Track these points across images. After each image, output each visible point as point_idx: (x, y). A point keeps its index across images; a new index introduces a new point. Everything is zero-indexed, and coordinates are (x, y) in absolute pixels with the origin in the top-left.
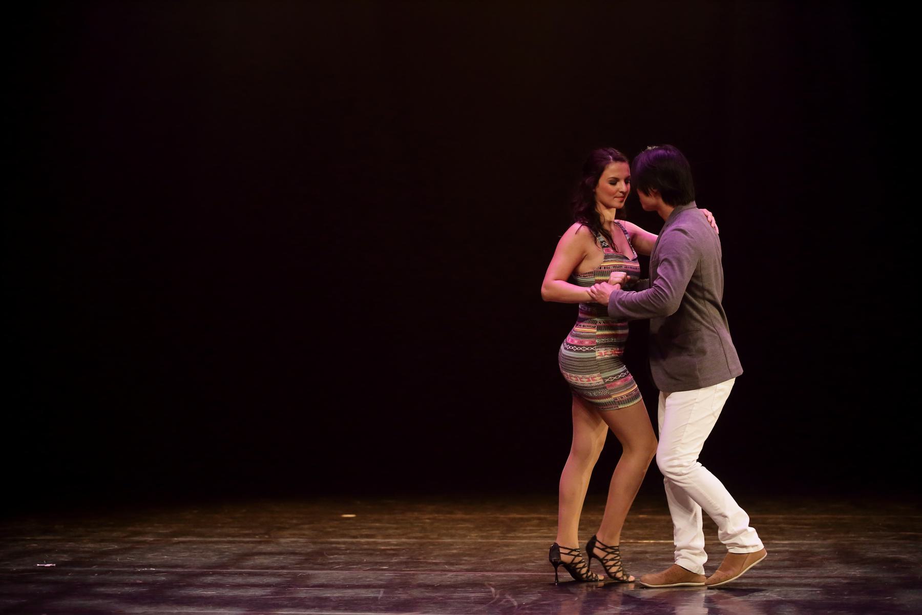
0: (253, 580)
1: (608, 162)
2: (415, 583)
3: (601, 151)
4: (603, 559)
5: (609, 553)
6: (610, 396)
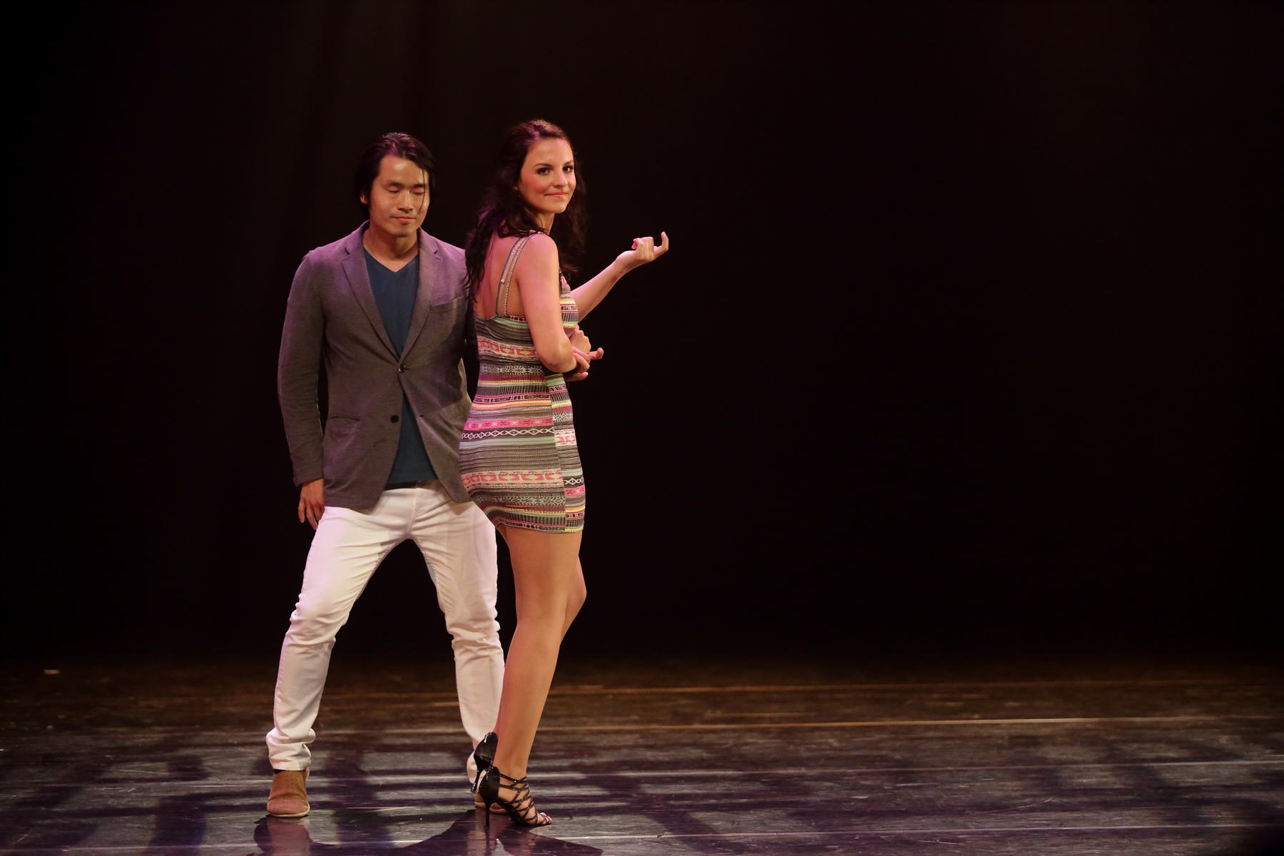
1: (386, 150)
2: (152, 817)
3: (524, 125)
4: (514, 801)
5: (519, 790)
6: (562, 508)
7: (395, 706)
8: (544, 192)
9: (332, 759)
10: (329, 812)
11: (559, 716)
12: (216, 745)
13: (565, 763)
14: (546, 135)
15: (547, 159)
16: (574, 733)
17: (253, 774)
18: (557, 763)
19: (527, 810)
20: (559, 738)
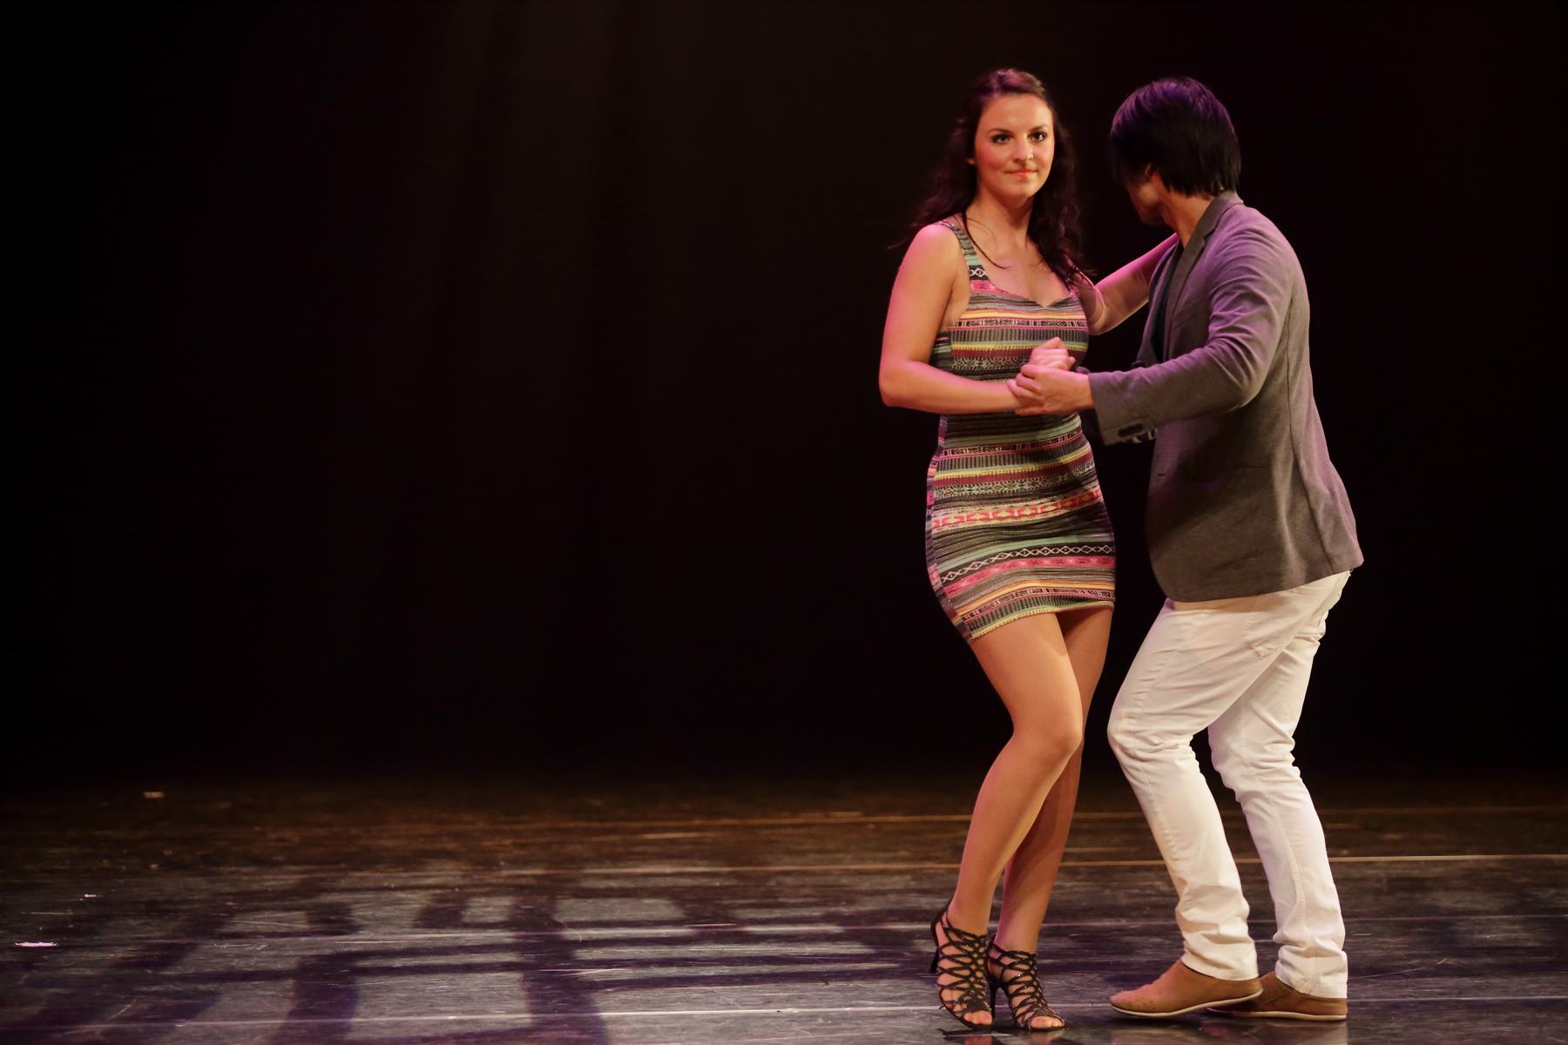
0: (790, 831)
7: (594, 839)
8: (996, 167)
9: (517, 907)
10: (516, 976)
11: (809, 851)
12: (368, 889)
13: (817, 912)
14: (1008, 89)
15: (1011, 122)
16: (826, 873)
17: (417, 926)
18: (805, 913)
19: (944, 971)
20: (808, 880)
